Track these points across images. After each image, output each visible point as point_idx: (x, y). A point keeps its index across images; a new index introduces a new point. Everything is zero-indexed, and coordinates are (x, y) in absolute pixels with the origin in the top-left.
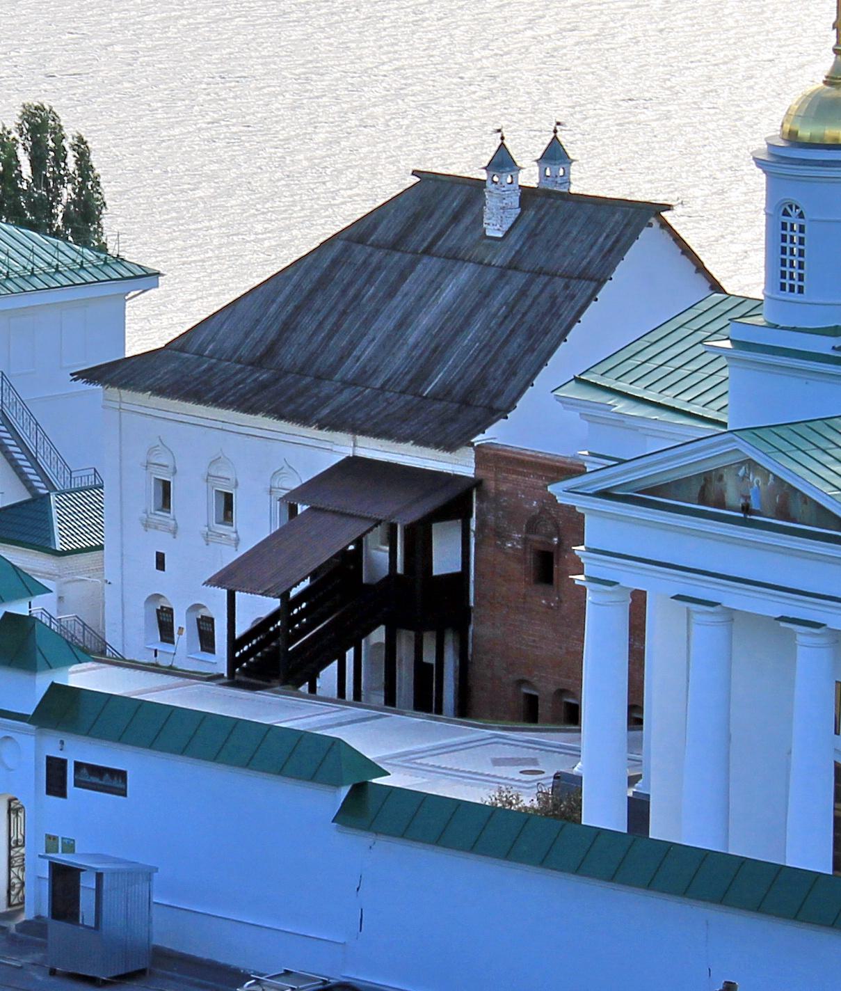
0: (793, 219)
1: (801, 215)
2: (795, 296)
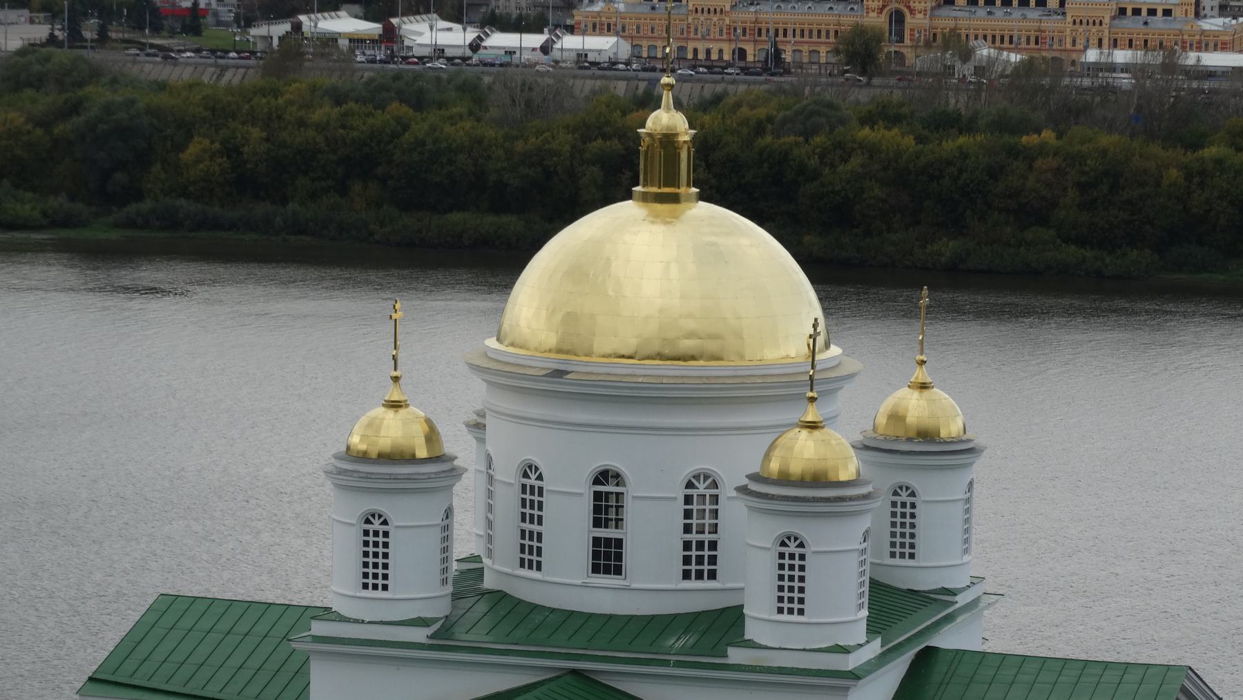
1: (385, 523)
2: (379, 594)
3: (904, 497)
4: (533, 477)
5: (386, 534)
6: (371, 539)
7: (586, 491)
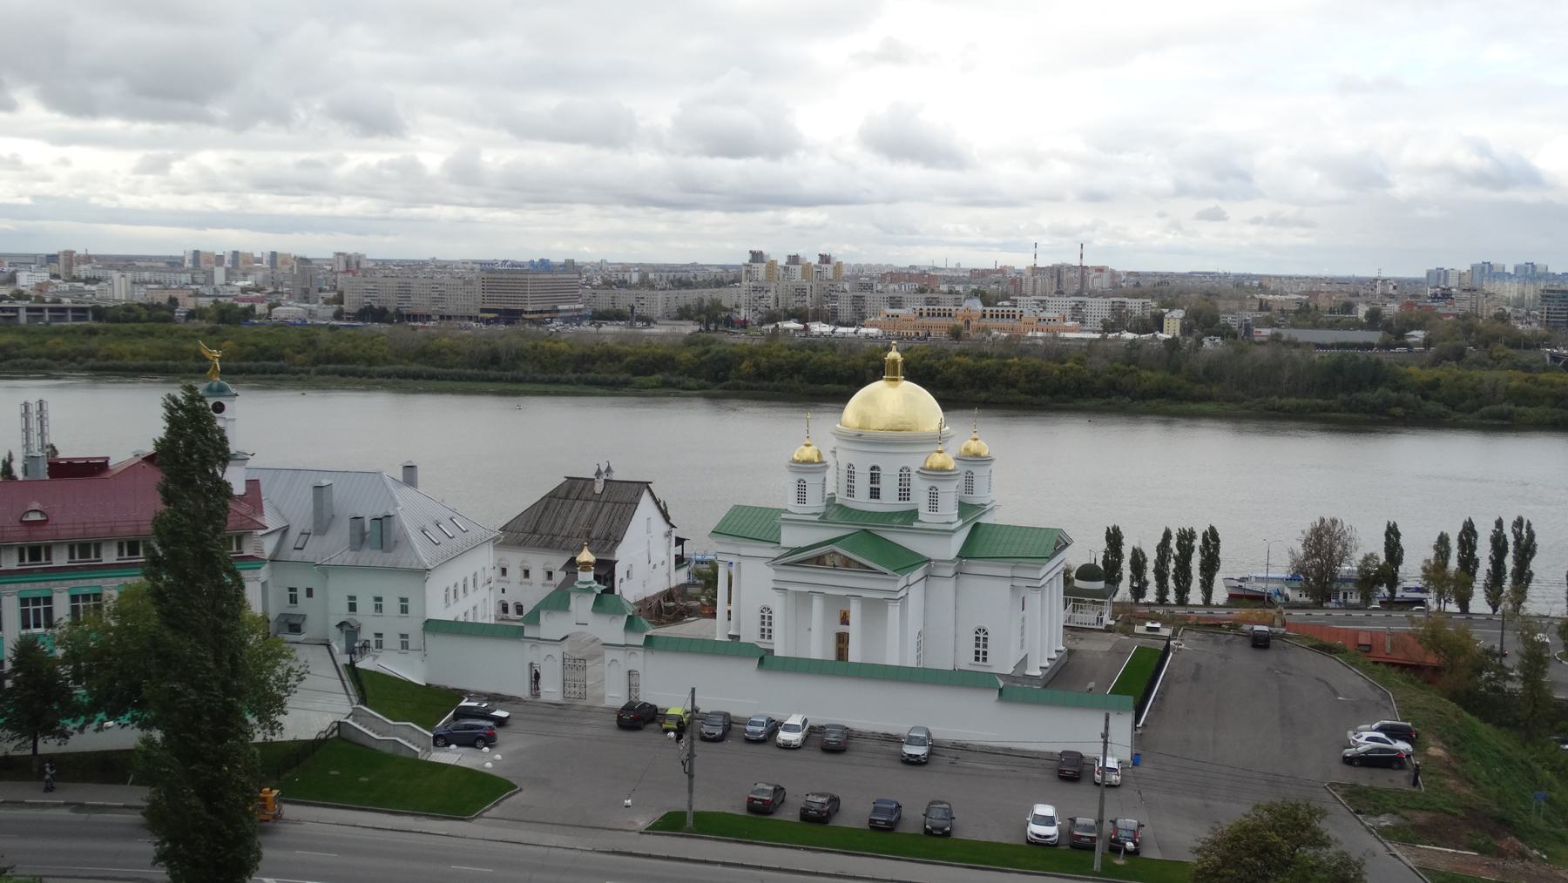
7: (868, 473)
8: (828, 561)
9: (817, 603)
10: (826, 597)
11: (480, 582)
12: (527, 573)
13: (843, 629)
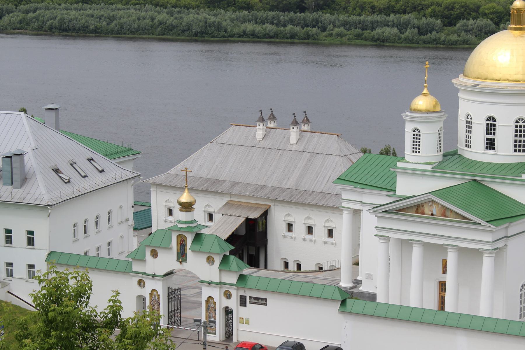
0: (417, 132)
1: (419, 132)
2: (418, 154)
3: (417, 132)
4: (469, 118)
5: (420, 135)
6: (415, 137)
7: (484, 123)
8: (427, 210)
9: (417, 251)
10: (426, 246)
11: (115, 220)
12: (310, 230)
13: (442, 277)
